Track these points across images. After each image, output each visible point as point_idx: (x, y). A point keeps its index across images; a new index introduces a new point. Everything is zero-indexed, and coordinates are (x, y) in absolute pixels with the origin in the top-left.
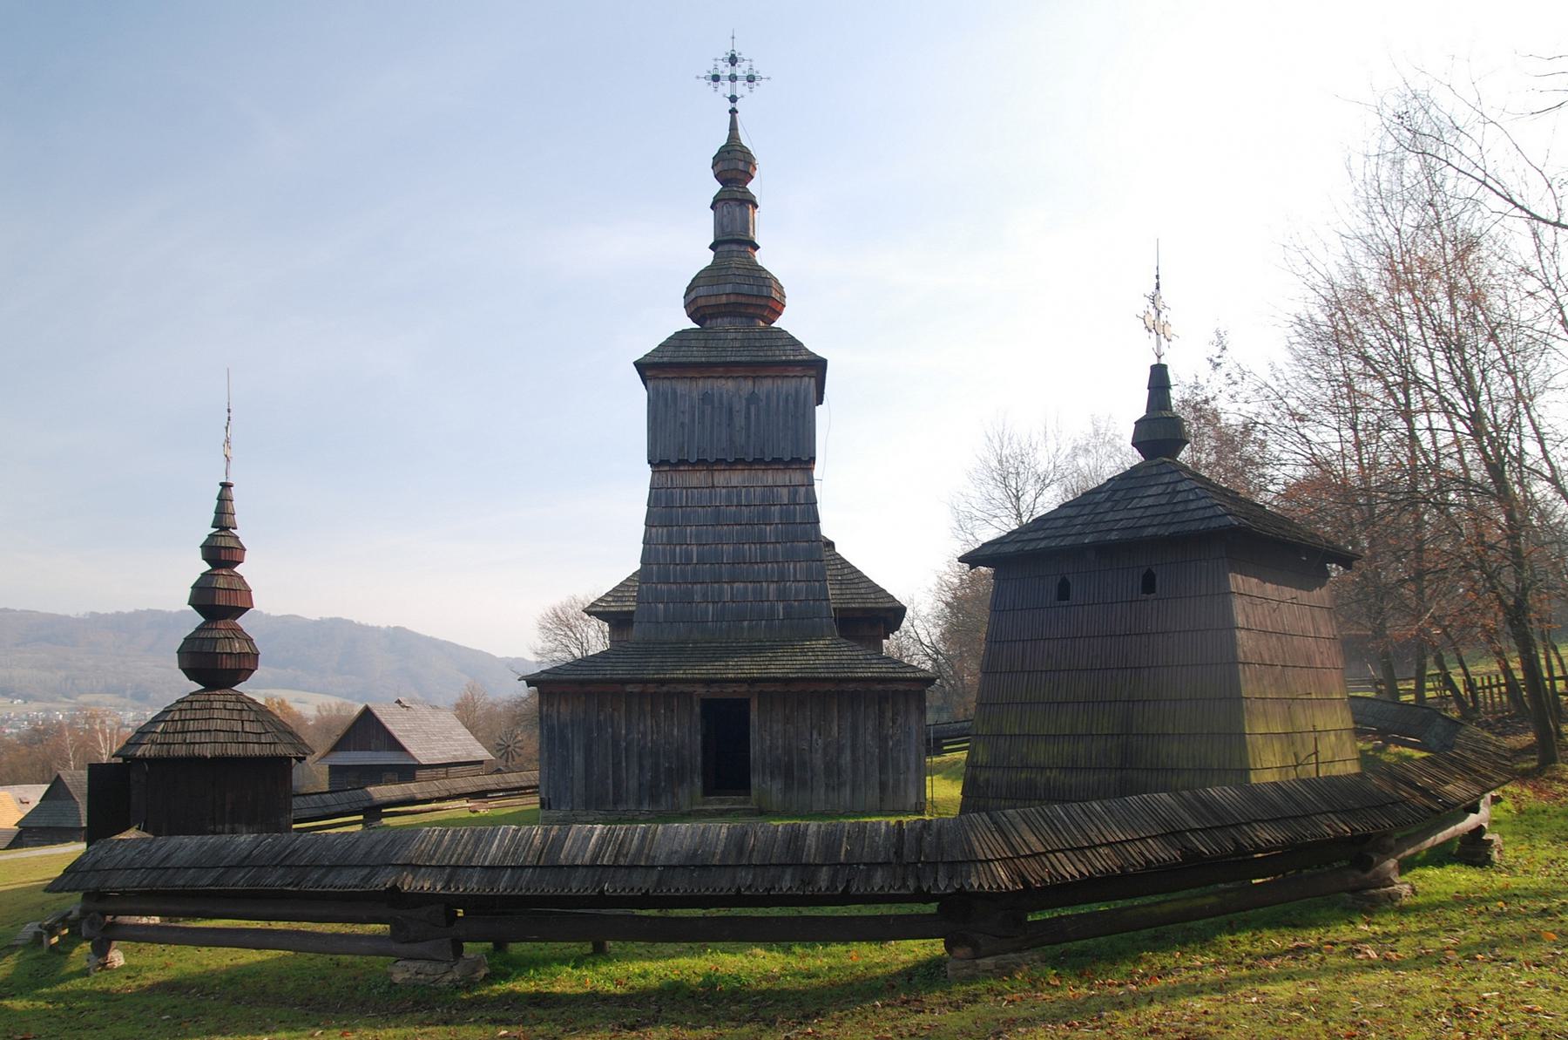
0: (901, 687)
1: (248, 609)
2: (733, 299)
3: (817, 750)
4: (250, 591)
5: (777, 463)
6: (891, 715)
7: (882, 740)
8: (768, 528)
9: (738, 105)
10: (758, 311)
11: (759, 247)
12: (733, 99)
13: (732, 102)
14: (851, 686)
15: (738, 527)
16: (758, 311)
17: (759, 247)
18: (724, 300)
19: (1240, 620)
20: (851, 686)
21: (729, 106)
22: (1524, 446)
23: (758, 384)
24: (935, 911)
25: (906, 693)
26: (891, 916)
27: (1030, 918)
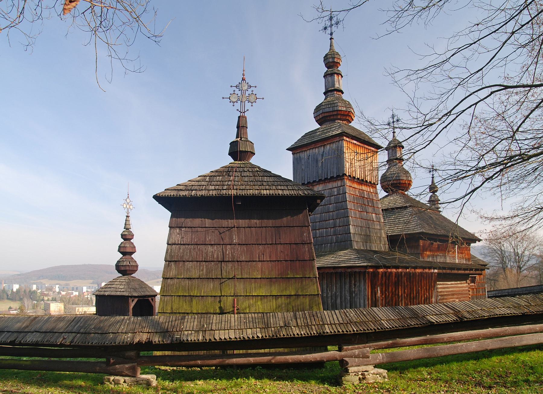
0: (357, 270)
1: (135, 252)
2: (323, 115)
3: (329, 297)
4: (135, 247)
5: (332, 179)
6: (354, 282)
7: (351, 293)
8: (330, 206)
9: (333, 36)
10: (335, 117)
11: (343, 93)
12: (331, 34)
13: (331, 35)
14: (340, 270)
15: (321, 207)
16: (335, 117)
17: (343, 93)
18: (321, 116)
19: (294, 217)
20: (340, 270)
21: (330, 37)
22: (341, 83)
23: (325, 147)
24: (105, 360)
25: (360, 273)
26: (75, 361)
27: (214, 368)
